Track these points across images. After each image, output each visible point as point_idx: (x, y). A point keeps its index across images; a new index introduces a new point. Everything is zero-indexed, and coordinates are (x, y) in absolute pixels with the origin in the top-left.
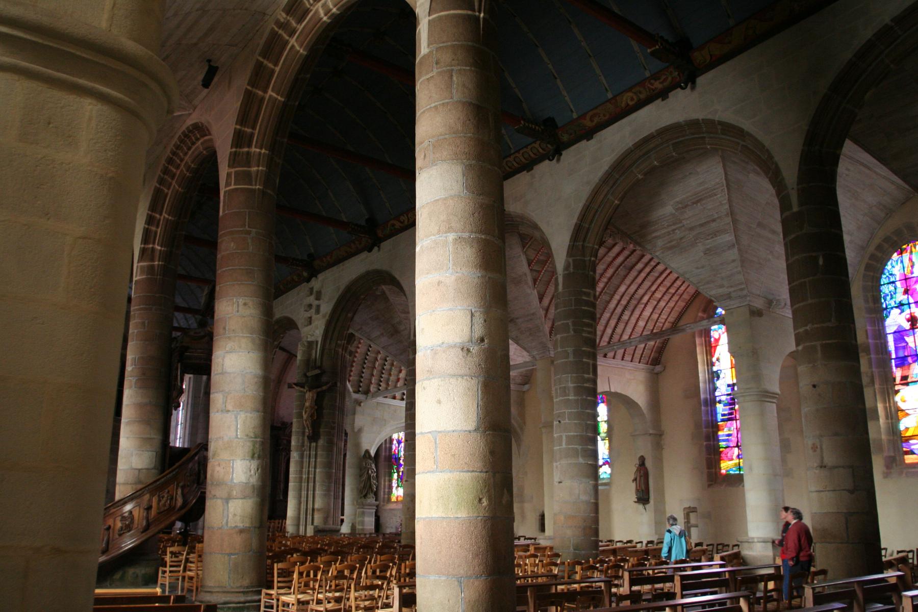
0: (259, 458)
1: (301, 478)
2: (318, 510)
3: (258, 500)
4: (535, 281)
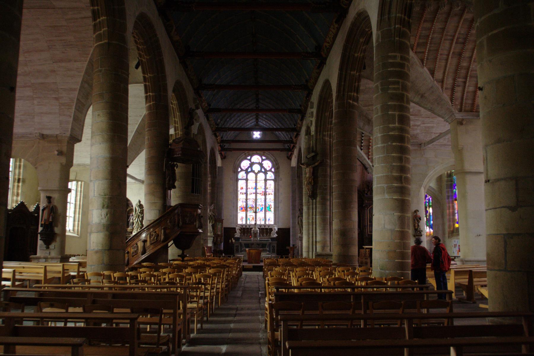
0: (107, 207)
1: (309, 222)
2: (319, 242)
3: (107, 233)
4: (422, 61)
